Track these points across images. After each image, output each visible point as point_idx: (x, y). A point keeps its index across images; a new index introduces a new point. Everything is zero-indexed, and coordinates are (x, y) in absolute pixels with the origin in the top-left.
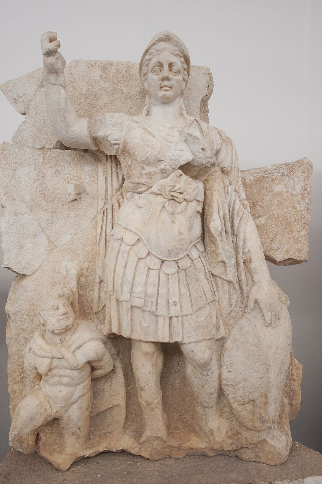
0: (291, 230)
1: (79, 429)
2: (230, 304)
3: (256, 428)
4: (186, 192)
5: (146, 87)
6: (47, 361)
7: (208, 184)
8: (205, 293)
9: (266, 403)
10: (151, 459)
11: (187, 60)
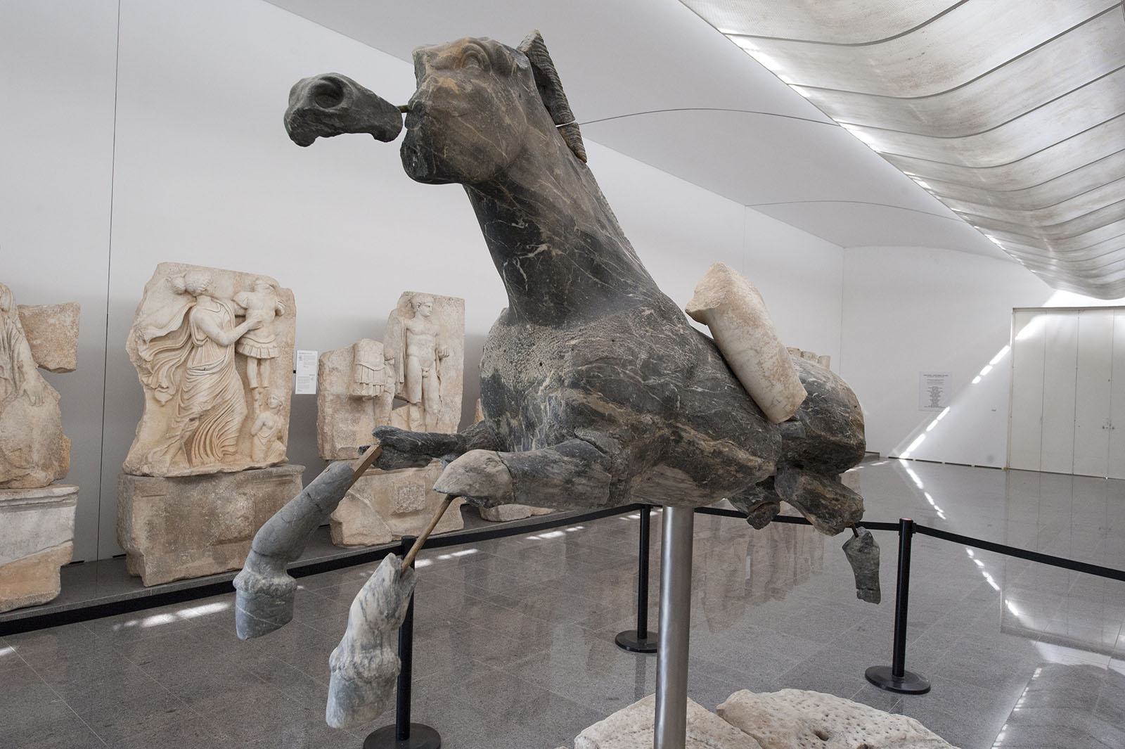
3: (22, 466)
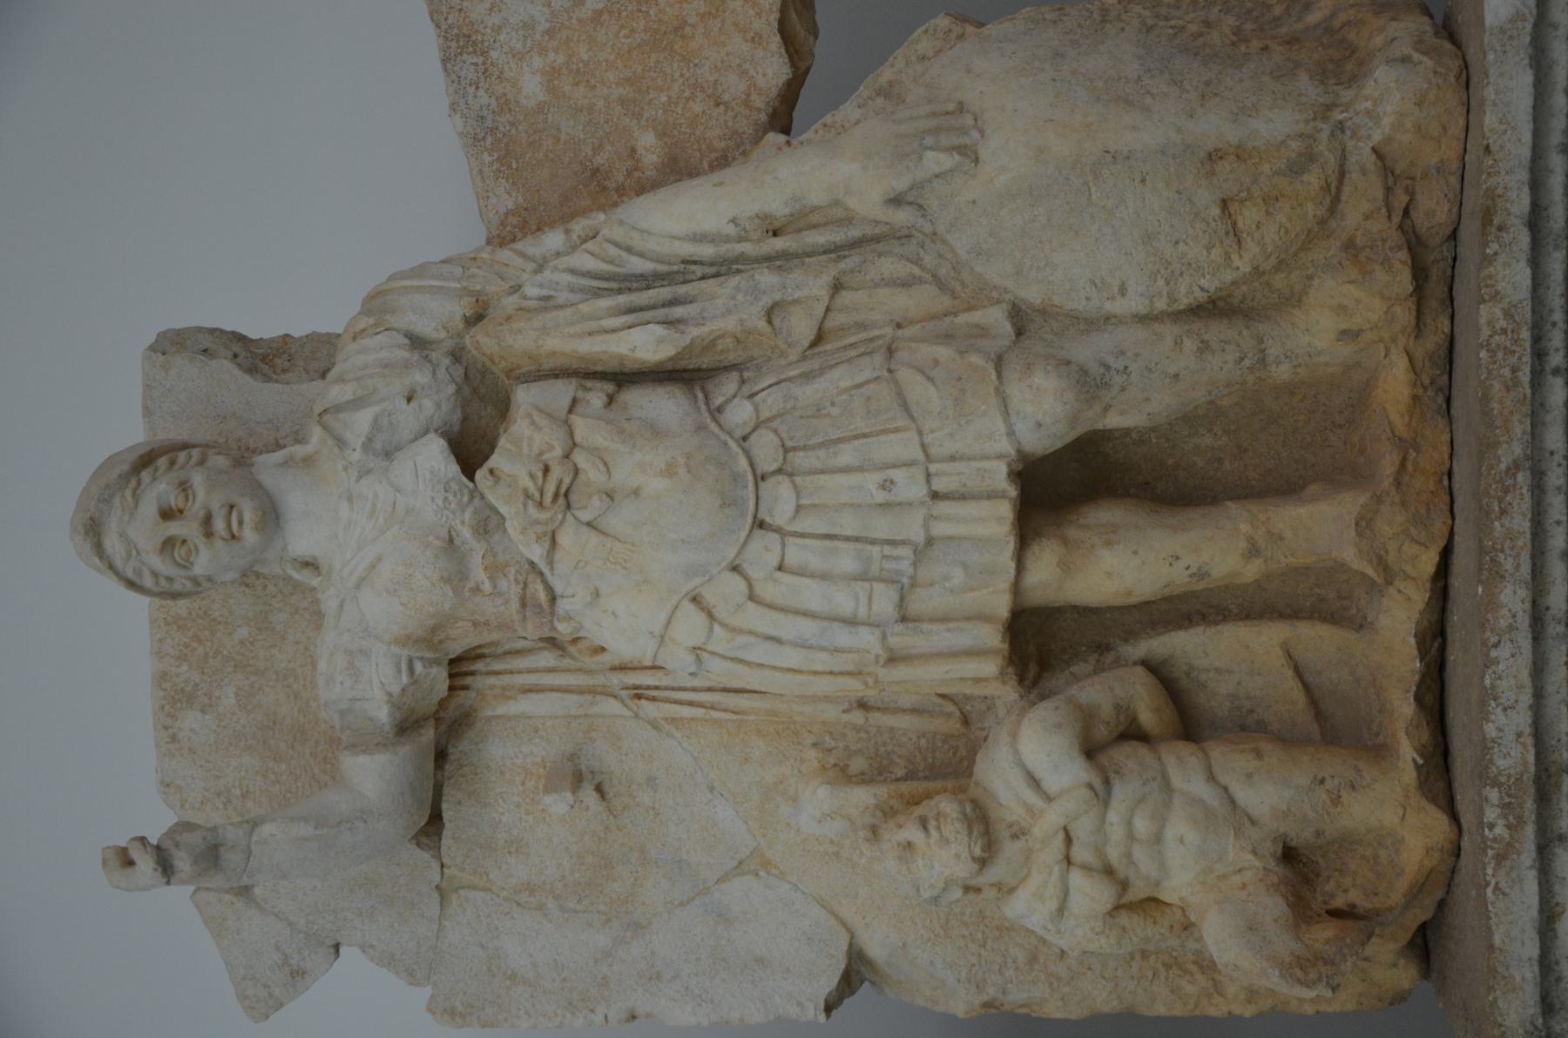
0: (676, 30)
1: (1322, 781)
2: (906, 284)
4: (541, 454)
5: (232, 575)
6: (1077, 878)
7: (519, 367)
8: (859, 386)
9: (1240, 153)
10: (1442, 544)
11: (146, 460)
